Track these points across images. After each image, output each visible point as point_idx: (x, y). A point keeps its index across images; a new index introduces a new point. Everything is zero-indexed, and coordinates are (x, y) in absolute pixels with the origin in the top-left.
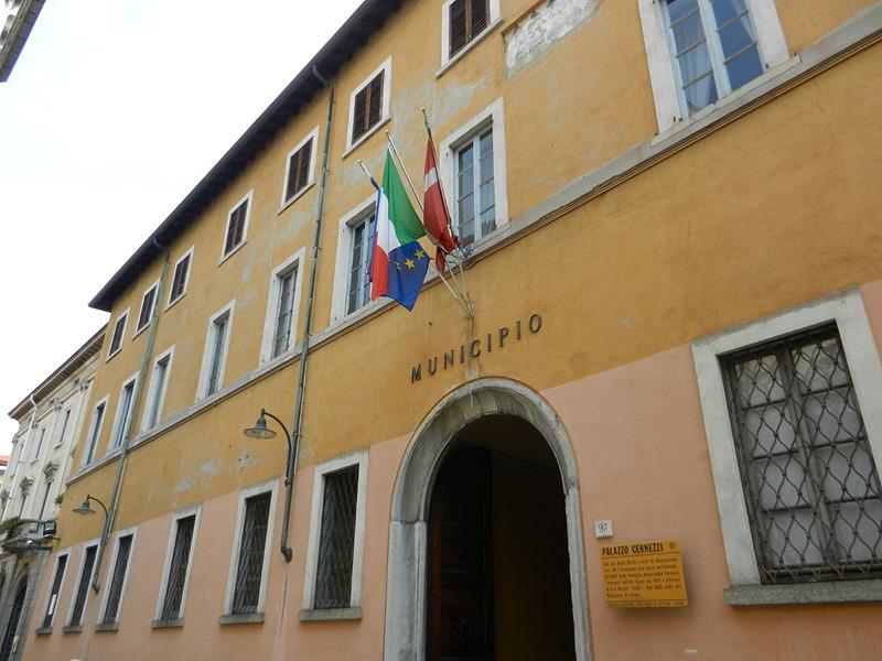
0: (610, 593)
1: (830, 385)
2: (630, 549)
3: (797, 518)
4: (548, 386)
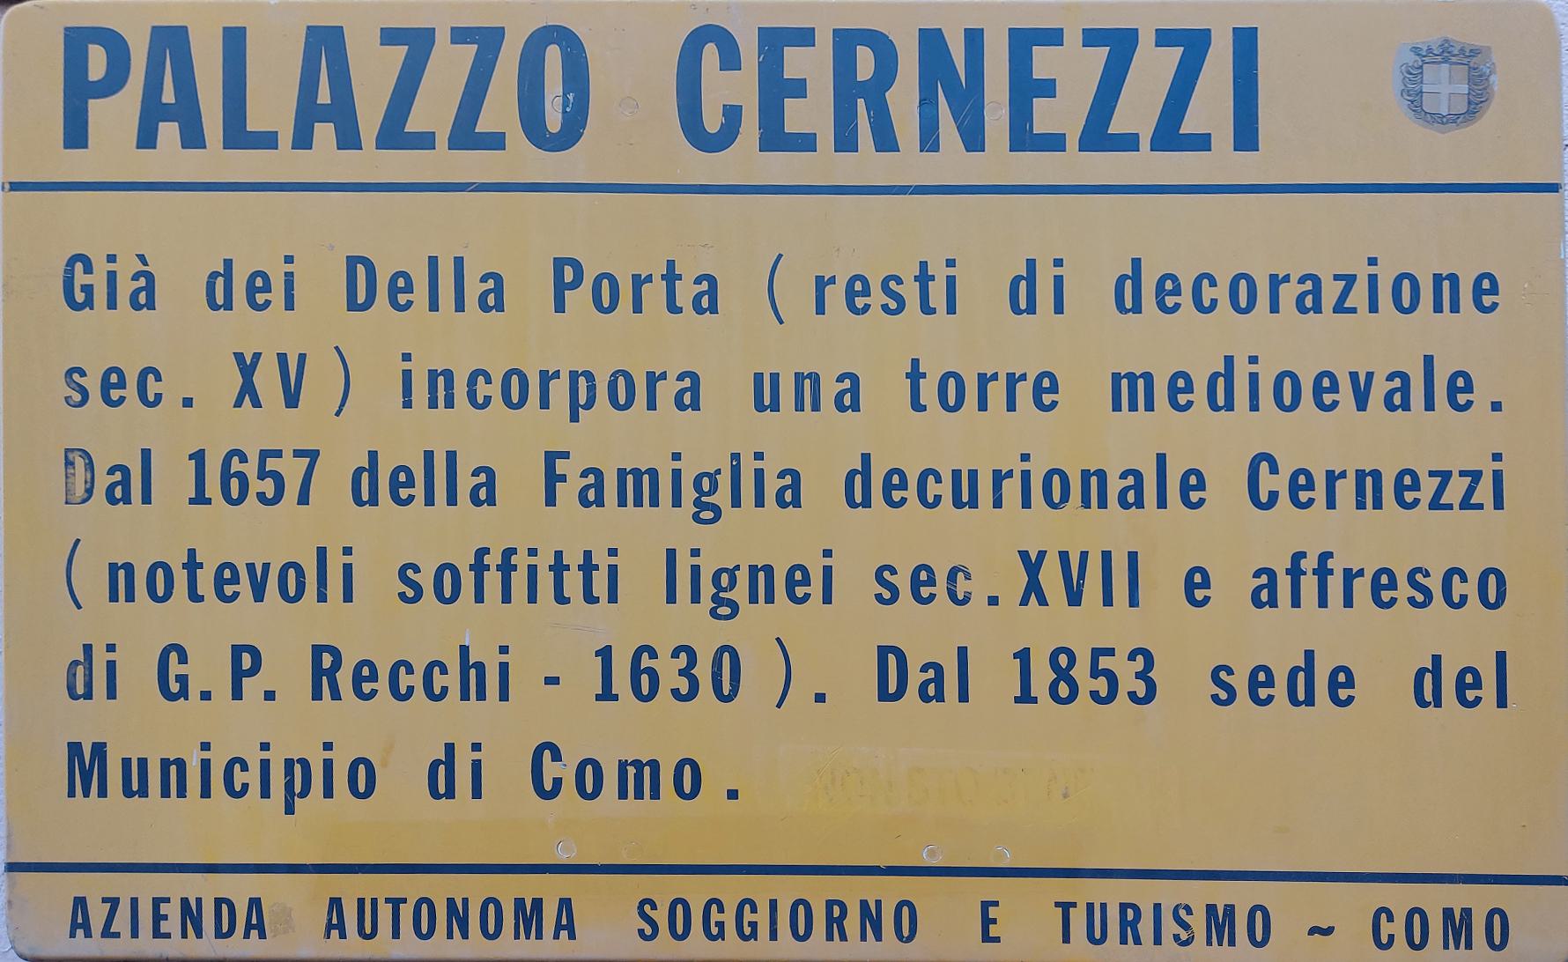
0: (137, 725)
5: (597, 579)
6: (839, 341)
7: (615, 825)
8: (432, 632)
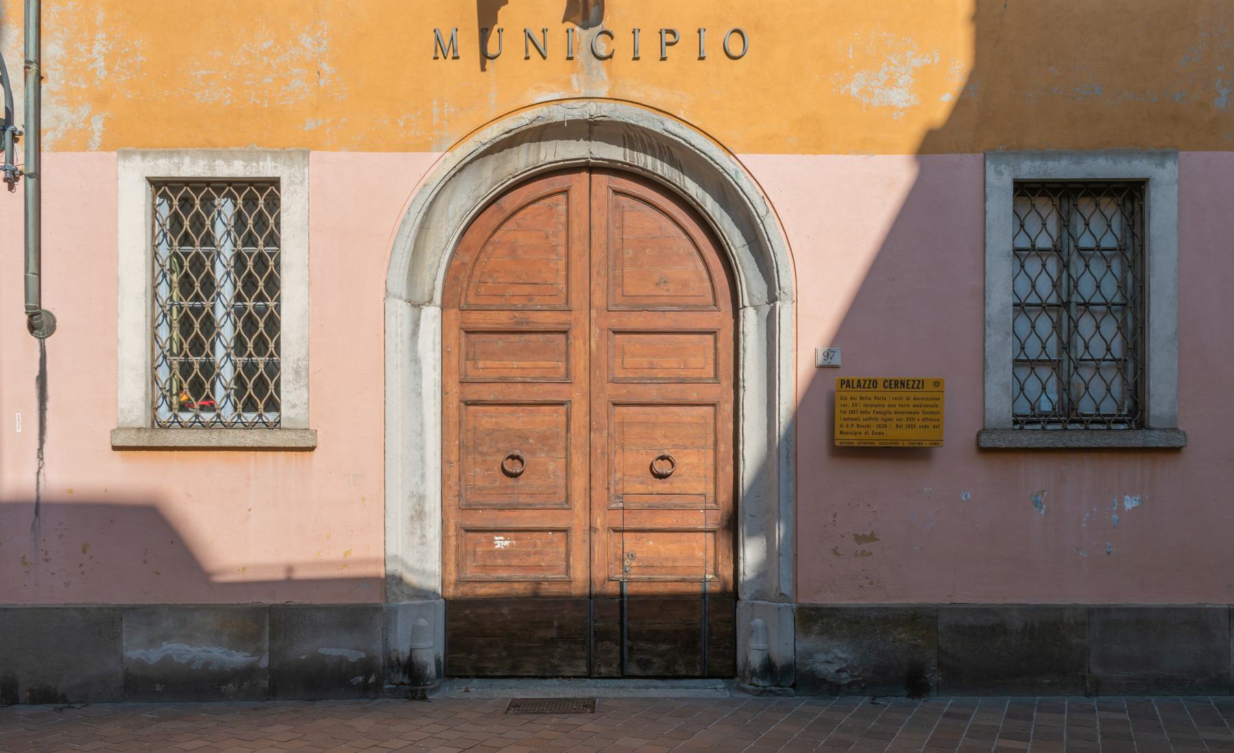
1: (1033, 246)
2: (880, 384)
3: (1037, 370)
4: (752, 149)
5: (876, 419)
6: (894, 402)
7: (877, 437)
8: (866, 423)
